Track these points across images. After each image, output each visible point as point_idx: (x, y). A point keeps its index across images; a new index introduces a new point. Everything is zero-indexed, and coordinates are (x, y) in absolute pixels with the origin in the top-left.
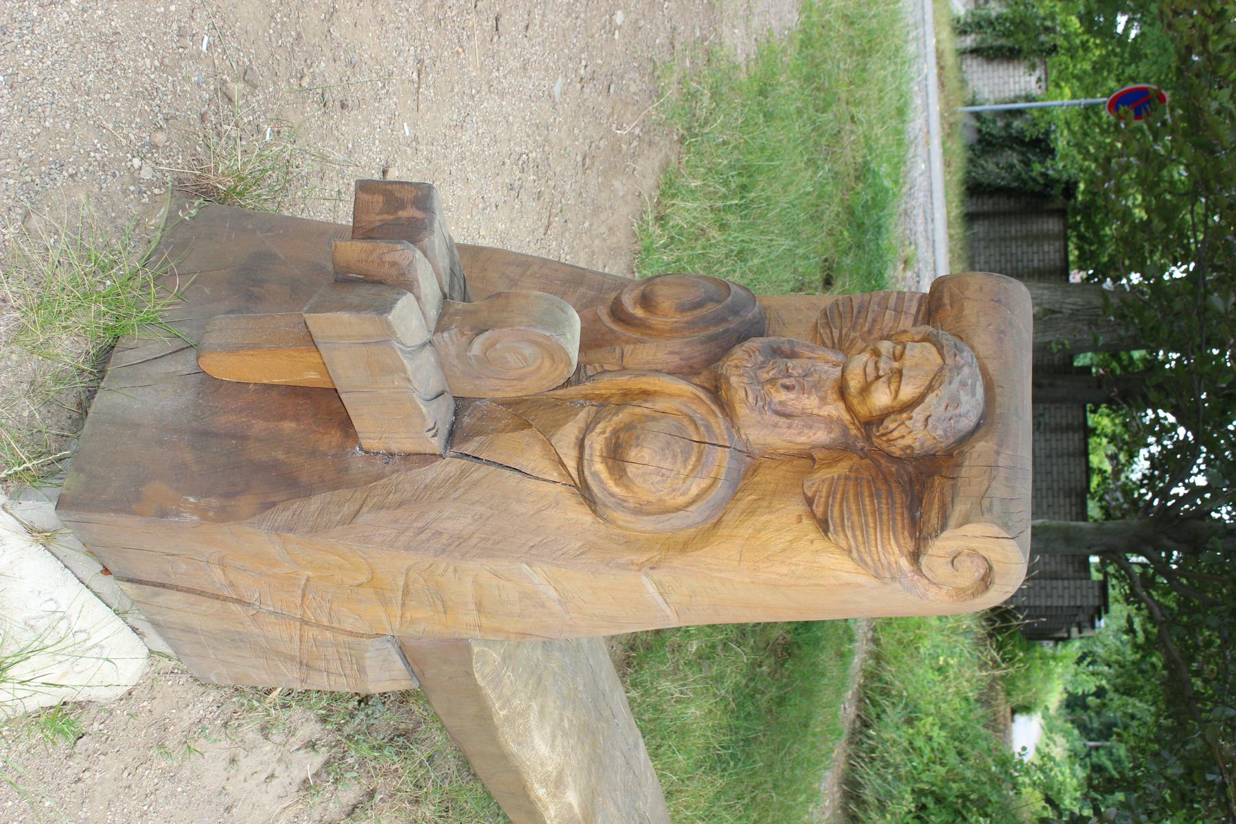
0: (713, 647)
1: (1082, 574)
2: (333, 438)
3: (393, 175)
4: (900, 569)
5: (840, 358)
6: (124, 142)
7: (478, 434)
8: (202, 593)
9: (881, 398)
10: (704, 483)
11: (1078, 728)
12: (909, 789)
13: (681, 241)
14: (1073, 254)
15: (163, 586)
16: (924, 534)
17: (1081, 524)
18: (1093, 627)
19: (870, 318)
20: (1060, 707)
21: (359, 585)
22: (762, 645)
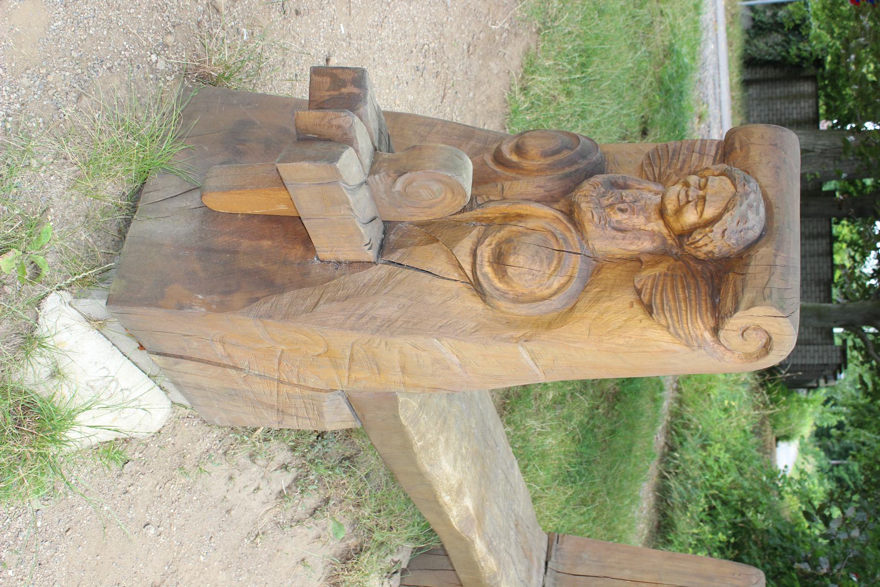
0: (564, 395)
1: (828, 341)
2: (298, 251)
3: (334, 62)
4: (704, 340)
5: (659, 188)
6: (145, 43)
7: (401, 247)
8: (208, 362)
9: (690, 217)
10: (563, 280)
11: (824, 451)
12: (703, 495)
13: (539, 106)
14: (822, 111)
15: (182, 357)
16: (722, 314)
17: (829, 305)
18: (835, 378)
19: (681, 159)
20: (811, 436)
21: (319, 355)
22: (599, 394)
